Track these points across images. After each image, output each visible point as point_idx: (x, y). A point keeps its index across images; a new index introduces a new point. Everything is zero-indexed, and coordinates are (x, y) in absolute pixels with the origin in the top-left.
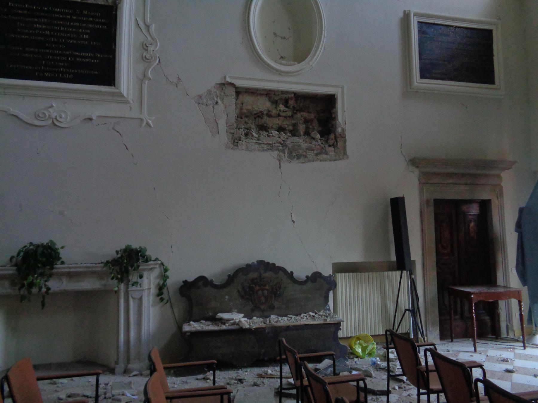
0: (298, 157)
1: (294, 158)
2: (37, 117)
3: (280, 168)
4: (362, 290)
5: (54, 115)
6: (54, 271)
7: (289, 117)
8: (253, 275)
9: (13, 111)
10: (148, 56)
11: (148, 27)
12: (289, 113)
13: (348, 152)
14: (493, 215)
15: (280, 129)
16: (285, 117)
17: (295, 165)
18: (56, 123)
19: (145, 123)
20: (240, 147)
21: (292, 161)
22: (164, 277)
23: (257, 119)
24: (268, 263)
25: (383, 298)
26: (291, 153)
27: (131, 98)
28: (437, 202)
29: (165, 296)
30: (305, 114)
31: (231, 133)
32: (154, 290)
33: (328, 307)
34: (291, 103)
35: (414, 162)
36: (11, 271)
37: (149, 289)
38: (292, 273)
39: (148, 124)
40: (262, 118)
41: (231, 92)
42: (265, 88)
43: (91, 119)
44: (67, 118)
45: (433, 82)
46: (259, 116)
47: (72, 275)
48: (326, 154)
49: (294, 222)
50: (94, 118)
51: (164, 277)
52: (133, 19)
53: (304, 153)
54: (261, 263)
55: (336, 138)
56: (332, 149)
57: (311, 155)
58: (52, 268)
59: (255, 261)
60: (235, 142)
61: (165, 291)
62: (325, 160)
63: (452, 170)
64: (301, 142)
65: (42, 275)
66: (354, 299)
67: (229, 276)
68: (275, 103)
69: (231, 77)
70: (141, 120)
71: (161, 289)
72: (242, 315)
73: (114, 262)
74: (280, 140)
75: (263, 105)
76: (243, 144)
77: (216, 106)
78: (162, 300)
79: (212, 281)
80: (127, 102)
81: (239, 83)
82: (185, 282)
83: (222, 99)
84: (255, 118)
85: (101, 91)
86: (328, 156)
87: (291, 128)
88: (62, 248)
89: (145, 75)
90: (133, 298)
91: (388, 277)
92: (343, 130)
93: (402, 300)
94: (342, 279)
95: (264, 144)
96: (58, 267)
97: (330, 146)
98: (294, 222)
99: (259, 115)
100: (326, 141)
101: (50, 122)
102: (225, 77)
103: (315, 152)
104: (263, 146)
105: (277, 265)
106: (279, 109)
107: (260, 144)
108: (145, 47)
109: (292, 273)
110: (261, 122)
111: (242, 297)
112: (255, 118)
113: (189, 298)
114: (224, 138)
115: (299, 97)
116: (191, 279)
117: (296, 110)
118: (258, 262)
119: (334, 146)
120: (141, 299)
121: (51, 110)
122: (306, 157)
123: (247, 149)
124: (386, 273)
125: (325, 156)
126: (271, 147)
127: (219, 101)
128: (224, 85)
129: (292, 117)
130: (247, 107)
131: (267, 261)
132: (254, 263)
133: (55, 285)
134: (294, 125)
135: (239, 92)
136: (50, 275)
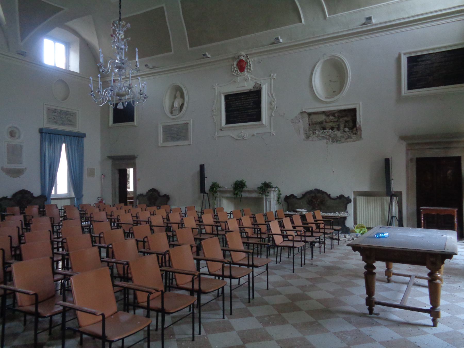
0: (337, 141)
1: (335, 141)
2: (238, 136)
3: (327, 147)
4: (370, 205)
5: (243, 135)
6: (244, 190)
7: (336, 121)
8: (313, 195)
9: (232, 135)
10: (272, 107)
11: (272, 95)
12: (336, 120)
13: (362, 136)
14: (199, 174)
15: (332, 128)
16: (334, 122)
17: (335, 145)
18: (244, 138)
19: (272, 134)
20: (309, 139)
21: (333, 144)
22: (280, 194)
23: (321, 124)
24: (319, 190)
25: (383, 210)
26: (333, 140)
27: (267, 125)
28: (419, 160)
29: (280, 201)
30: (345, 118)
31: (306, 134)
32: (276, 199)
33: (346, 211)
34: (336, 115)
35: (403, 138)
36: (232, 189)
37: (274, 198)
38: (330, 195)
39: (273, 134)
40: (323, 124)
41: (306, 115)
42: (321, 111)
43: (254, 135)
44: (247, 135)
45: (411, 92)
46: (322, 123)
47: (250, 192)
48: (351, 138)
49: (333, 172)
50: (255, 134)
51: (280, 194)
52: (267, 93)
53: (340, 139)
54: (316, 190)
55: (357, 130)
56: (355, 135)
57: (343, 140)
58: (243, 189)
59: (314, 189)
60: (308, 137)
61: (280, 200)
62: (350, 141)
63: (428, 141)
64: (338, 134)
65: (239, 191)
66: (366, 210)
67: (303, 195)
68: (328, 116)
69: (304, 109)
70: (271, 133)
71: (279, 198)
72: (306, 210)
73: (261, 188)
74: (328, 134)
75: (323, 118)
76: (311, 138)
77: (299, 123)
78: (279, 203)
79: (296, 196)
80: (265, 127)
81: (309, 111)
82: (286, 196)
83: (302, 119)
84: (320, 124)
85: (256, 124)
86: (352, 140)
87: (337, 127)
88: (206, 177)
89: (271, 115)
90: (268, 201)
91: (386, 199)
92: (360, 125)
93: (49, 150)
94: (360, 200)
95: (320, 137)
96: (245, 189)
97: (354, 134)
98: (333, 172)
99: (321, 123)
100: (352, 132)
101: (242, 138)
102: (302, 110)
103: (345, 138)
104: (320, 138)
105: (323, 191)
106: (330, 119)
107: (318, 137)
108: (271, 104)
109: (330, 195)
110: (322, 125)
111: (308, 204)
112: (320, 124)
113: (287, 202)
114: (303, 136)
115: (341, 111)
116: (288, 195)
117: (339, 117)
118: (315, 189)
119: (356, 134)
120: (271, 202)
121: (242, 134)
122: (340, 141)
123: (312, 140)
124: (385, 197)
125: (350, 140)
126: (323, 138)
127: (301, 121)
128: (302, 113)
129: (337, 121)
130: (314, 120)
131: (319, 189)
132: (313, 190)
133: (244, 195)
134: (339, 125)
135: (309, 114)
136: (242, 191)
